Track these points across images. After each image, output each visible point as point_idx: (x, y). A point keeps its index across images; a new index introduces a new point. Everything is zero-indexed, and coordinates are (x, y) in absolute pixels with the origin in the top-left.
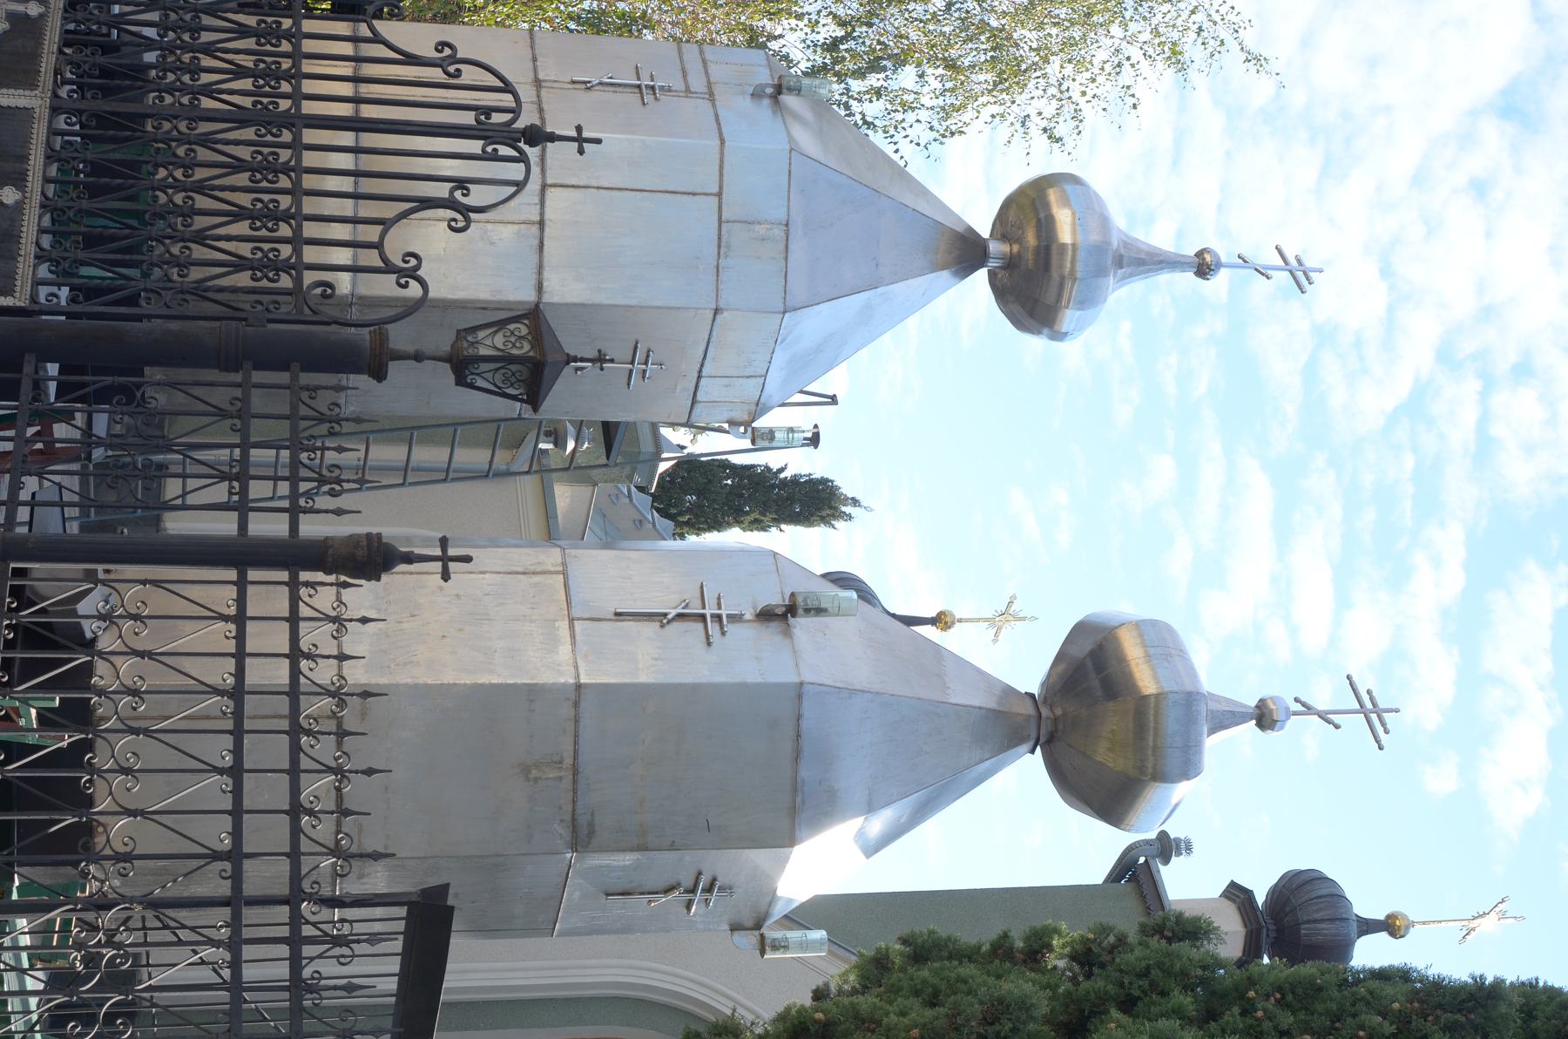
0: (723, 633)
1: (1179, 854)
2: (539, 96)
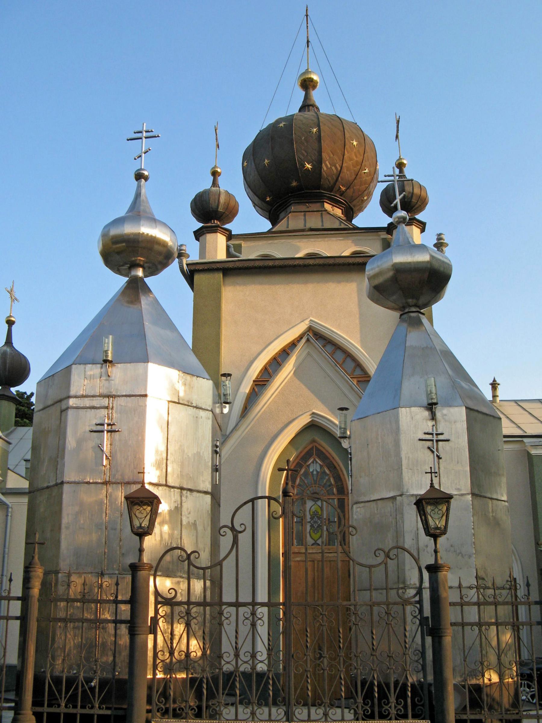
0: (442, 434)
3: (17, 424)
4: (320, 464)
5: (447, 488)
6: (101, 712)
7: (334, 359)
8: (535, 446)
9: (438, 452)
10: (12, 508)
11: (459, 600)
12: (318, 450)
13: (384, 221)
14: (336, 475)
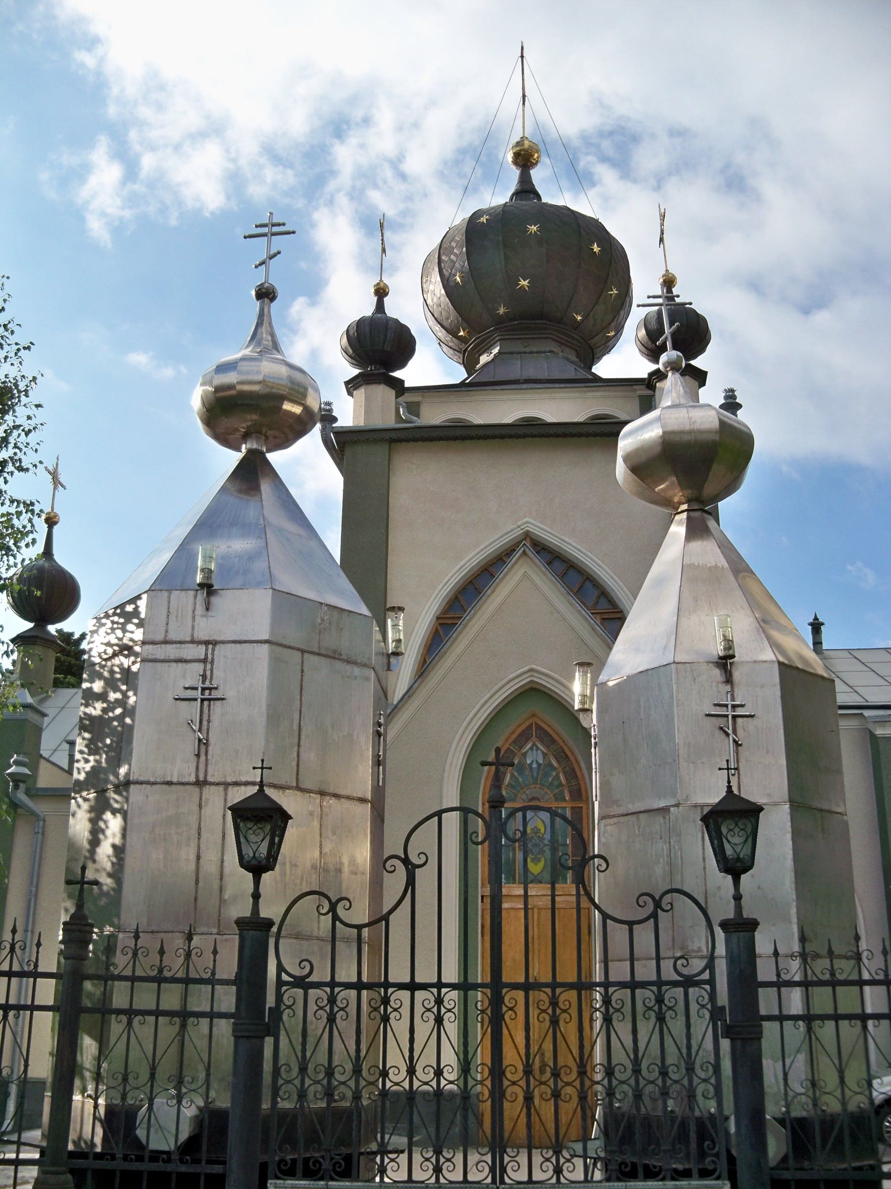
0: (742, 706)
1: (331, 410)
2: (218, 784)
3: (57, 684)
4: (543, 752)
5: (752, 792)
6: (183, 1169)
7: (565, 583)
8: (882, 722)
9: (736, 735)
10: (44, 821)
11: (774, 979)
12: (538, 727)
13: (642, 368)
14: (568, 768)
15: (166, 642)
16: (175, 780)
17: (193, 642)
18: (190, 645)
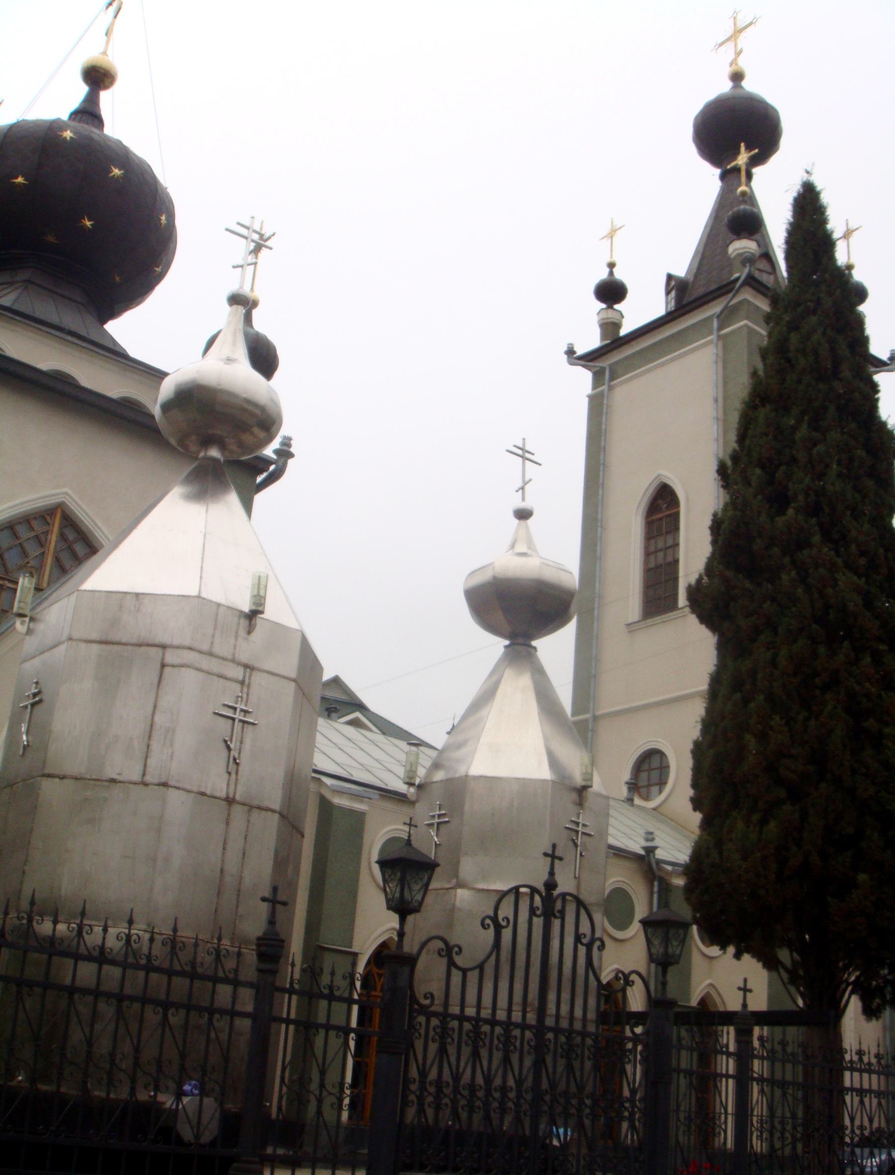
15: (211, 654)
16: (208, 792)
17: (233, 661)
18: (231, 664)
